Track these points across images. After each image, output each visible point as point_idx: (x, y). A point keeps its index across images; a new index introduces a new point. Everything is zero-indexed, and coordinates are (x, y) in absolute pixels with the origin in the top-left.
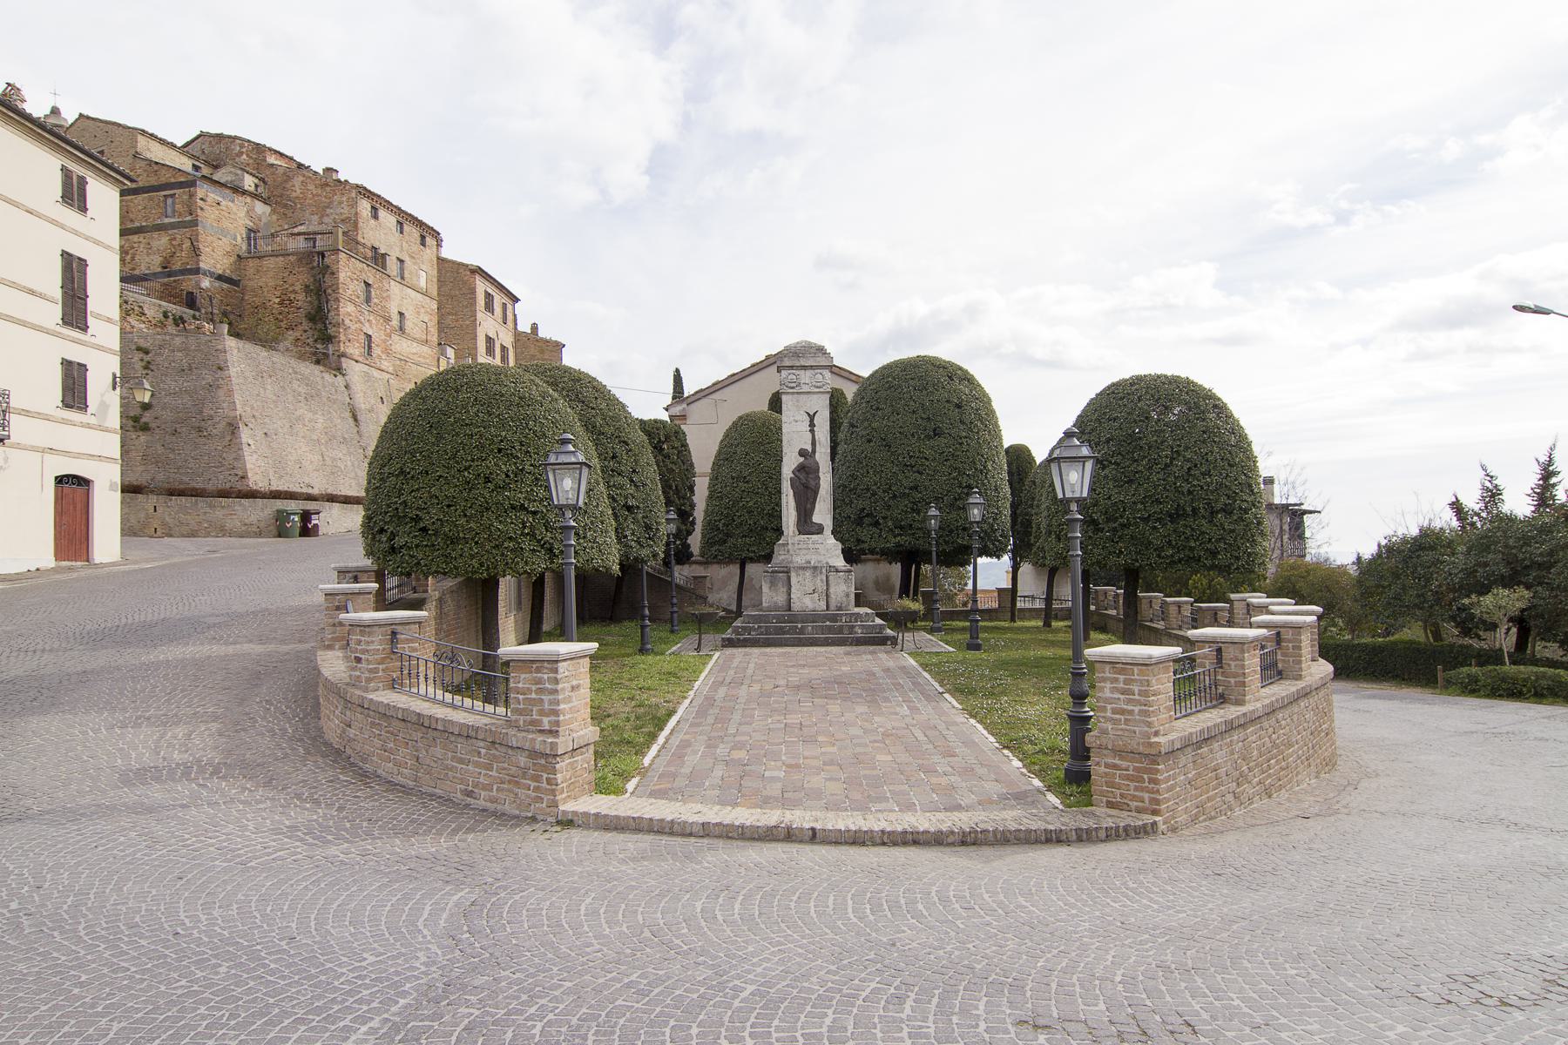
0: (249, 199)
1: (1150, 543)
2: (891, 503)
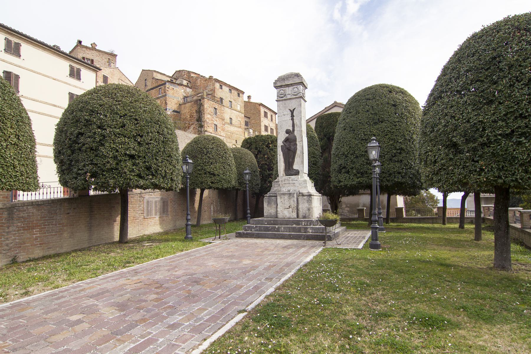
0: (184, 87)
1: (514, 158)
2: (355, 160)
